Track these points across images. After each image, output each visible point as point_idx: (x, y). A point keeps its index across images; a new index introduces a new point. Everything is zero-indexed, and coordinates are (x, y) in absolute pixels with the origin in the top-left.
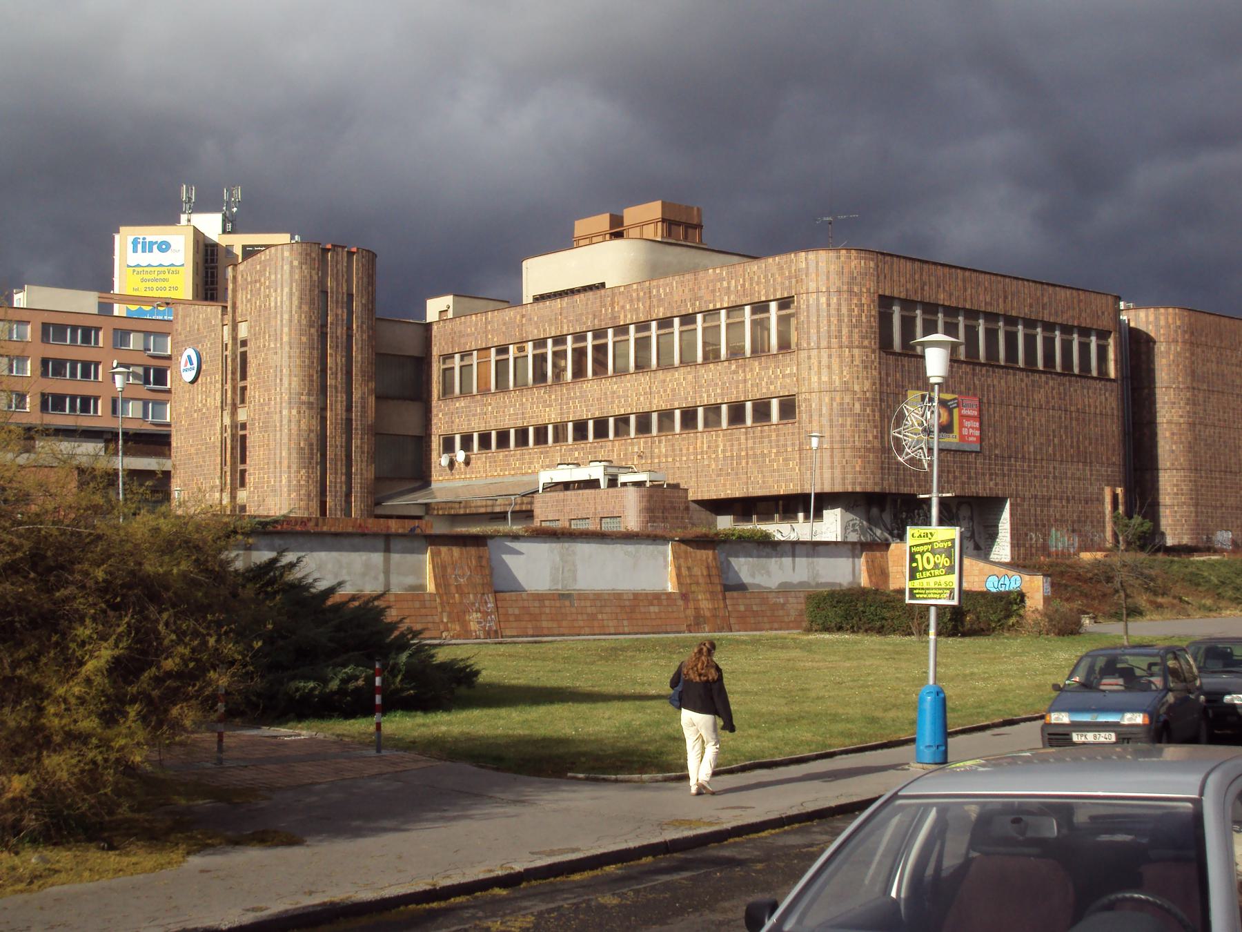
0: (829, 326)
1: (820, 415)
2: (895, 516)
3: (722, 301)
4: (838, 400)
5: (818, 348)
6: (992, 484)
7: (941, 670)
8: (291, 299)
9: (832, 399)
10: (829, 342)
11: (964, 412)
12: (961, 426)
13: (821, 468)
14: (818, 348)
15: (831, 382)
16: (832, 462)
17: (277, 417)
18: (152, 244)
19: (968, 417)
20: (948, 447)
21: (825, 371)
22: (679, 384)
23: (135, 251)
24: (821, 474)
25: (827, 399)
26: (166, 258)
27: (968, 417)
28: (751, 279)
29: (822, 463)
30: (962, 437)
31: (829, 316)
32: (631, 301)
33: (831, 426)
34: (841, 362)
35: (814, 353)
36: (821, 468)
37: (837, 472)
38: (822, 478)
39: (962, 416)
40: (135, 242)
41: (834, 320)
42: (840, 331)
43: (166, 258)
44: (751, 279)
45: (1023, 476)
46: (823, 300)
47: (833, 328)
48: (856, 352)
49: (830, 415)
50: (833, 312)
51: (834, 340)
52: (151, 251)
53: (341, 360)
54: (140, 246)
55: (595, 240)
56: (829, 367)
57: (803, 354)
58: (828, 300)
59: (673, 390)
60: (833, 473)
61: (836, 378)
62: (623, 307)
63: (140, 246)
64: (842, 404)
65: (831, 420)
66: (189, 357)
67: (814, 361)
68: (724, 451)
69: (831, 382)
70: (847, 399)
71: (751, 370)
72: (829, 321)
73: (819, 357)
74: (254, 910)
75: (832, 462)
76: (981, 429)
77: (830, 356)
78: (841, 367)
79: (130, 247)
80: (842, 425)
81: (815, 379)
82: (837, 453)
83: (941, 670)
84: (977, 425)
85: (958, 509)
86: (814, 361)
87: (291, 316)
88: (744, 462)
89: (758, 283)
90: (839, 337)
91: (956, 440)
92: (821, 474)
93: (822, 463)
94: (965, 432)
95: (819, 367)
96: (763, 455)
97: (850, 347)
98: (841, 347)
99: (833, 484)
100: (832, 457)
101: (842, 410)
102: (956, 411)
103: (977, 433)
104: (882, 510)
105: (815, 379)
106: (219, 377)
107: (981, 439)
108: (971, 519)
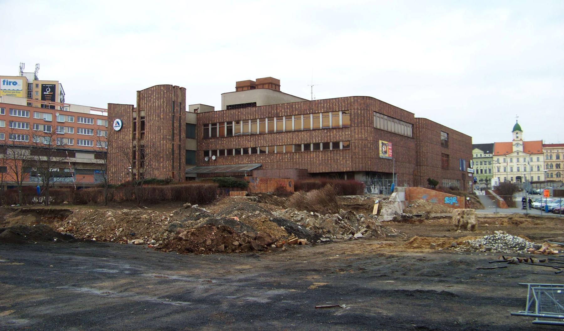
3: (321, 110)
17: (159, 143)
18: (10, 82)
22: (304, 136)
23: (4, 84)
26: (15, 88)
28: (333, 104)
32: (284, 109)
37: (364, 165)
40: (4, 81)
43: (15, 88)
44: (333, 104)
46: (359, 112)
52: (10, 84)
54: (6, 83)
55: (244, 89)
57: (353, 128)
59: (301, 138)
62: (281, 111)
63: (6, 83)
66: (118, 122)
67: (356, 130)
68: (322, 157)
69: (362, 137)
71: (333, 133)
74: (37, 263)
79: (2, 83)
81: (357, 136)
86: (356, 130)
87: (164, 109)
88: (330, 161)
89: (336, 105)
90: (364, 123)
96: (337, 159)
106: (131, 129)
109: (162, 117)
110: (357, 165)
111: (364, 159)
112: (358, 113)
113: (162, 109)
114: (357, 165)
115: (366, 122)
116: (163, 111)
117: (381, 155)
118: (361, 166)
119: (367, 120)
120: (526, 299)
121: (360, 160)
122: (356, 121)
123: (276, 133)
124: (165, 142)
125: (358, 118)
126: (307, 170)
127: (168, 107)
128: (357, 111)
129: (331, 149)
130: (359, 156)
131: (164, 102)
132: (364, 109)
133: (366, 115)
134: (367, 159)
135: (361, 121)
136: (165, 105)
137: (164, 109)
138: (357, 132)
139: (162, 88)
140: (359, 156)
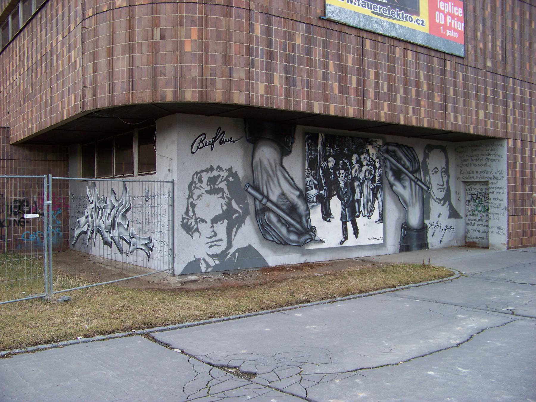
2: (313, 164)
7: (13, 180)
13: (110, 52)
16: (131, 38)
20: (408, 37)
24: (111, 65)
29: (112, 41)
36: (110, 52)
37: (142, 58)
38: (111, 74)
53: (478, 184)
60: (131, 61)
75: (131, 38)
83: (13, 180)
85: (426, 156)
91: (425, 29)
92: (111, 65)
93: (112, 41)
94: (439, 18)
99: (131, 86)
103: (460, 26)
104: (285, 151)
108: (446, 171)
110: (103, 61)
114: (103, 61)
118: (121, 66)
121: (121, 22)
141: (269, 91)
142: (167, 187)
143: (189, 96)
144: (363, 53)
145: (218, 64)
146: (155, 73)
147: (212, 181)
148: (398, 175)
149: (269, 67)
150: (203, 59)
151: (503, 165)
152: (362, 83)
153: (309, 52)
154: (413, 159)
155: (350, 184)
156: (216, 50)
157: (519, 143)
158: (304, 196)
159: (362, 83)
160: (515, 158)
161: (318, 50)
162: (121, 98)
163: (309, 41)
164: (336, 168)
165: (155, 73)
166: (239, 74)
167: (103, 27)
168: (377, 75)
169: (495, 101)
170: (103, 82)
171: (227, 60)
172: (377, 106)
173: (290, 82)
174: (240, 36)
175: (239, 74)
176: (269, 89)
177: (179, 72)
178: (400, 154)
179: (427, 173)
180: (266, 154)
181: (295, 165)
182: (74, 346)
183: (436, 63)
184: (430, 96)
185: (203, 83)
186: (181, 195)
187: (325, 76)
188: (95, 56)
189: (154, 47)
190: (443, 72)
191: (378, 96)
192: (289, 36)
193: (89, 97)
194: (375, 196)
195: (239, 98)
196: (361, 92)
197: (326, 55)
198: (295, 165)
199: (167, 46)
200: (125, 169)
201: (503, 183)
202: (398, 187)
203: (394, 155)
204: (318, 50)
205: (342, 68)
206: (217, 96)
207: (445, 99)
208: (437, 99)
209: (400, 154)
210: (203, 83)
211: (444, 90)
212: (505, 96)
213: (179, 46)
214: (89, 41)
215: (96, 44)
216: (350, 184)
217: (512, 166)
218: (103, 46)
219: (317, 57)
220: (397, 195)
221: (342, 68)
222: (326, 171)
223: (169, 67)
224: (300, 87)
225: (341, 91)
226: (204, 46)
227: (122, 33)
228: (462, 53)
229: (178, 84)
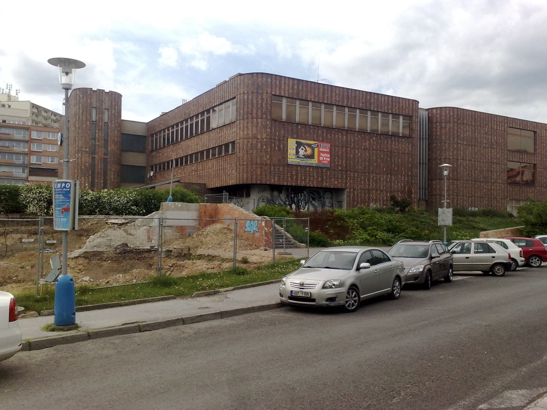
0: (248, 109)
1: (243, 149)
2: (287, 196)
4: (250, 142)
5: (243, 119)
6: (336, 182)
8: (79, 110)
9: (248, 142)
10: (248, 116)
11: (321, 150)
12: (319, 156)
13: (243, 173)
14: (243, 119)
15: (248, 134)
16: (247, 170)
19: (323, 152)
21: (245, 129)
24: (243, 175)
25: (246, 142)
27: (323, 152)
30: (319, 161)
31: (248, 104)
33: (247, 154)
34: (252, 125)
35: (242, 121)
37: (249, 175)
38: (243, 177)
39: (319, 152)
41: (250, 106)
42: (252, 111)
45: (261, 168)
47: (249, 110)
48: (259, 120)
49: (247, 149)
50: (250, 102)
51: (250, 115)
56: (247, 127)
58: (248, 97)
60: (247, 175)
61: (250, 132)
64: (252, 144)
65: (247, 152)
69: (248, 134)
70: (254, 142)
72: (248, 107)
73: (243, 123)
76: (331, 157)
77: (248, 123)
78: (252, 127)
80: (252, 154)
82: (250, 167)
84: (329, 156)
85: (324, 194)
87: (79, 117)
90: (252, 114)
91: (316, 162)
92: (243, 175)
93: (243, 170)
94: (321, 158)
95: (243, 128)
97: (257, 118)
98: (252, 118)
99: (247, 180)
100: (247, 168)
101: (252, 147)
102: (316, 150)
105: (241, 133)
107: (330, 162)
108: (332, 198)
109: (77, 126)
110: (241, 174)
111: (250, 167)
112: (244, 99)
113: (77, 117)
114: (241, 174)
115: (254, 111)
116: (79, 119)
117: (292, 159)
118: (245, 176)
119: (257, 109)
120: (62, 179)
121: (245, 167)
122: (242, 111)
123: (399, 115)
124: (80, 155)
125: (244, 107)
126: (205, 184)
127: (84, 113)
128: (244, 97)
129: (223, 155)
130: (243, 162)
131: (79, 108)
132: (252, 93)
133: (255, 101)
134: (254, 166)
135: (248, 111)
136: (81, 112)
137: (79, 117)
138: (242, 128)
139: (78, 92)
140: (243, 162)
141: (275, 181)
142: (253, 200)
143: (258, 182)
144: (297, 170)
145: (264, 176)
146: (252, 178)
147: (263, 199)
148: (314, 199)
149: (274, 176)
150: (261, 175)
151: (345, 196)
152: (297, 177)
153: (284, 172)
154: (319, 195)
155: (298, 201)
156: (264, 173)
157: (352, 190)
158: (285, 203)
159: (297, 177)
160: (350, 195)
161: (286, 171)
162: (245, 182)
163: (284, 169)
164: (294, 197)
165: (252, 178)
166: (268, 178)
167: (241, 168)
168: (301, 175)
169: (342, 178)
170: (241, 179)
171: (266, 175)
172: (300, 182)
173: (279, 179)
174: (269, 170)
175: (268, 178)
176: (274, 181)
177: (257, 178)
178: (315, 193)
179: (324, 198)
180: (276, 193)
181: (283, 196)
182: (137, 336)
183: (320, 170)
184: (317, 179)
185: (261, 180)
186: (256, 202)
187: (287, 177)
188: (239, 173)
189: (252, 172)
190: (322, 172)
191: (301, 180)
192: (279, 169)
193: (238, 181)
194: (306, 205)
195: (268, 183)
196: (297, 180)
197: (288, 172)
198: (283, 196)
199: (254, 172)
200: (241, 196)
201: (345, 201)
202: (313, 202)
203: (312, 193)
204: (286, 171)
205: (292, 175)
206: (264, 183)
207: (322, 179)
208: (320, 179)
209: (315, 193)
210: (261, 180)
211: (322, 177)
212: (346, 176)
213: (257, 173)
214: (238, 170)
215: (239, 171)
216: (298, 201)
217: (349, 196)
218: (241, 172)
219: (286, 173)
220: (313, 205)
221: (292, 175)
222: (291, 198)
223: (254, 177)
224: (281, 179)
225: (291, 180)
226: (261, 172)
227: (245, 169)
228: (329, 166)
229: (256, 181)
